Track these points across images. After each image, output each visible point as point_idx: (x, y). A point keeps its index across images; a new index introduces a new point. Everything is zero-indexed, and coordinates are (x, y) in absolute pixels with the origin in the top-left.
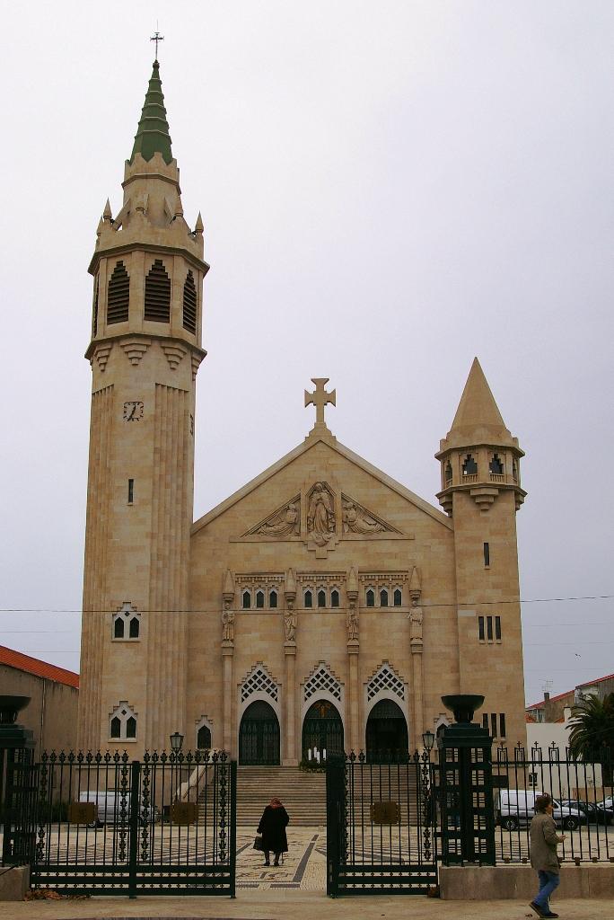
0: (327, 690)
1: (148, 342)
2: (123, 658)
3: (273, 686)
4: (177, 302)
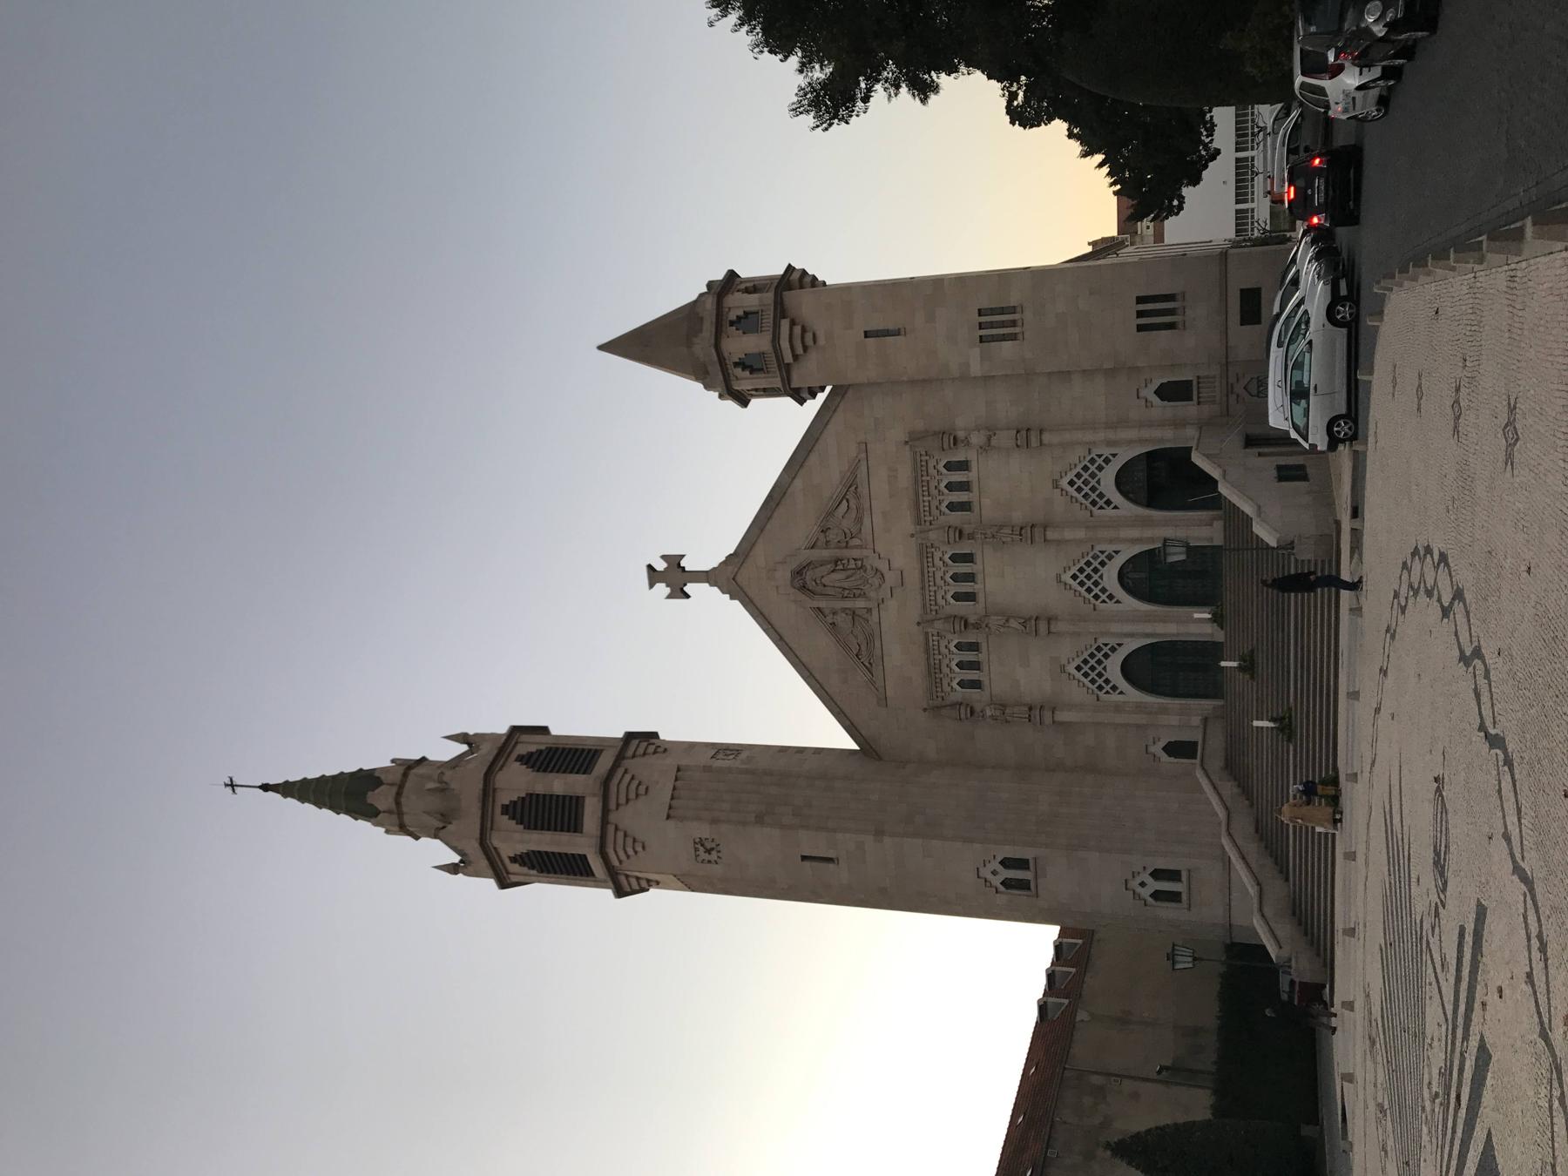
0: (1103, 570)
1: (611, 829)
2: (1057, 877)
3: (1095, 557)
4: (559, 784)
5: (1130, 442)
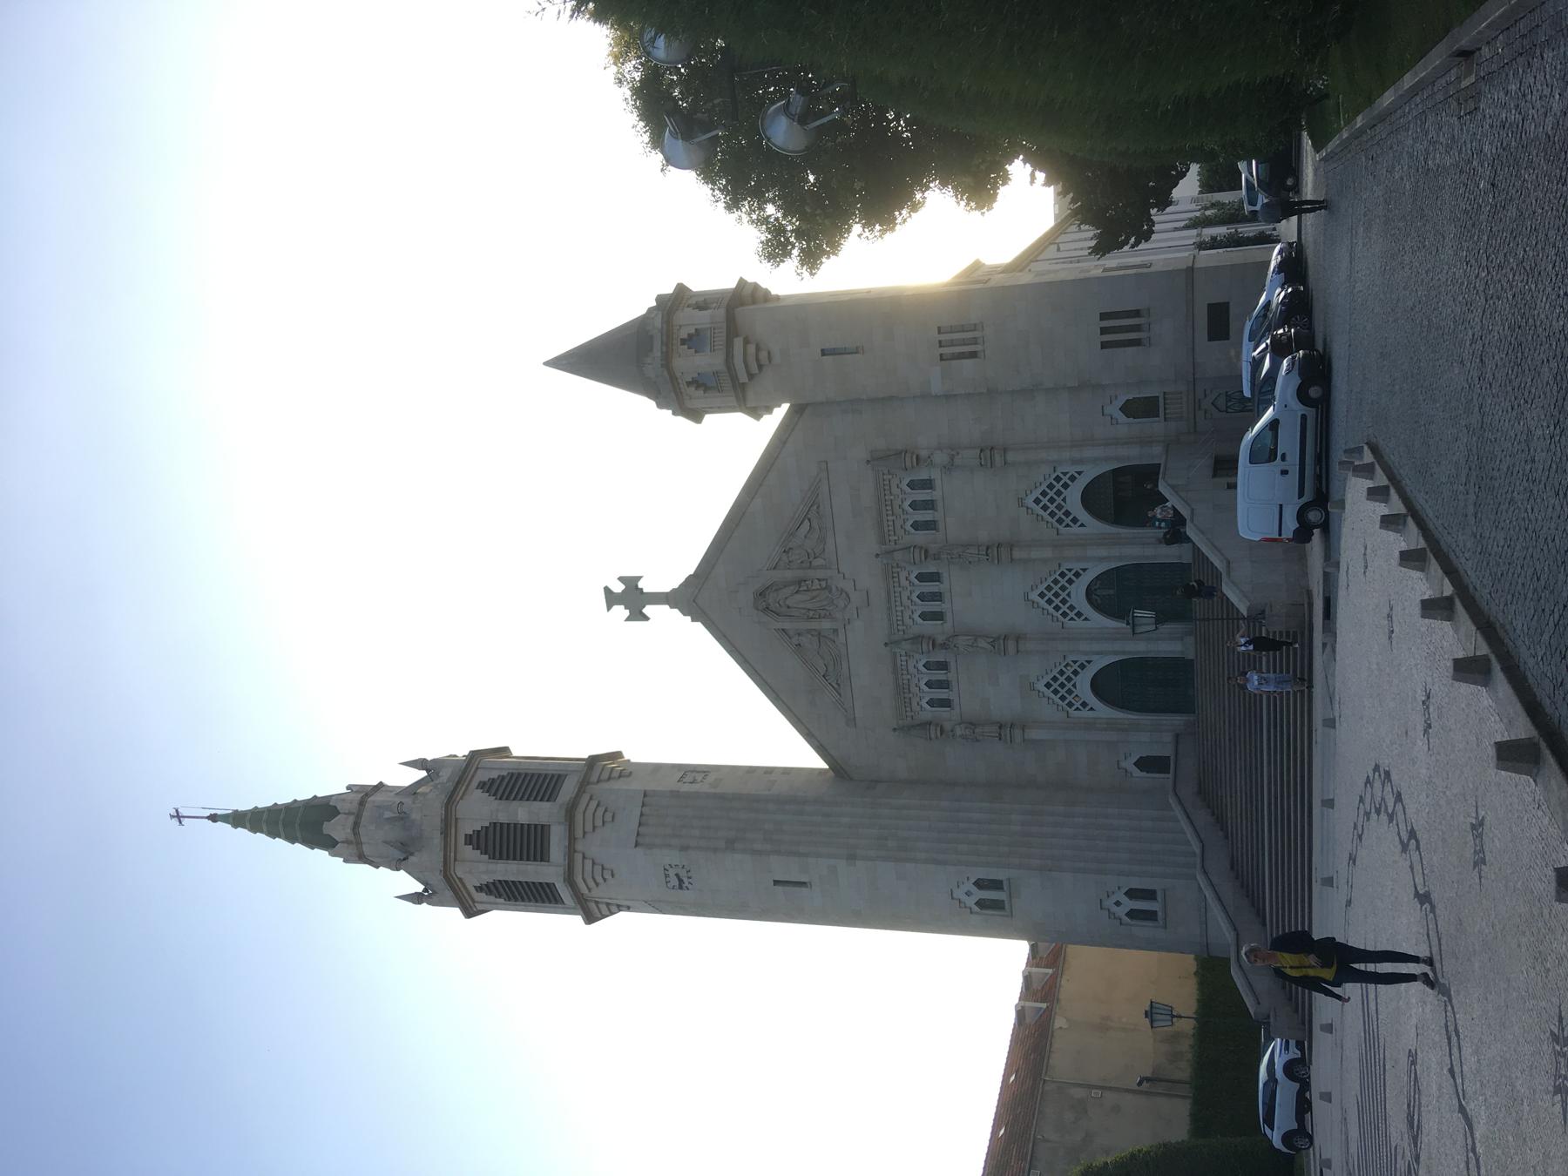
1: (578, 857)
3: (1062, 575)
4: (523, 813)
5: (1101, 559)
